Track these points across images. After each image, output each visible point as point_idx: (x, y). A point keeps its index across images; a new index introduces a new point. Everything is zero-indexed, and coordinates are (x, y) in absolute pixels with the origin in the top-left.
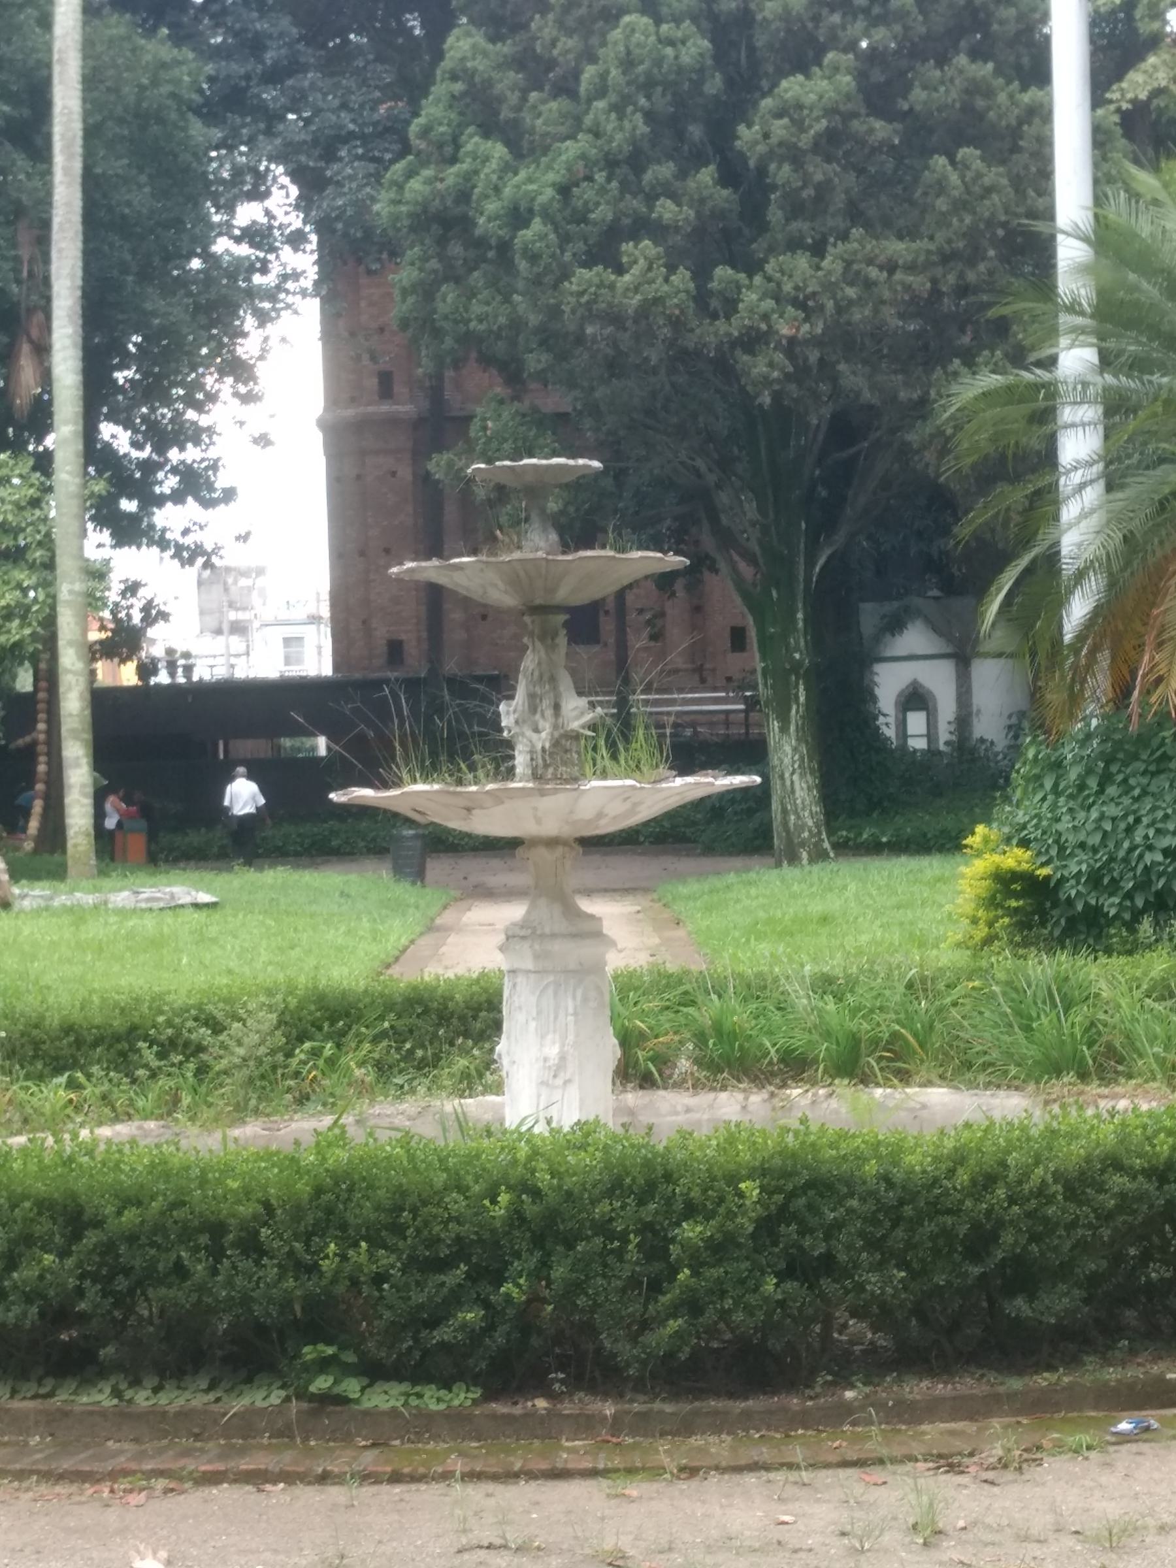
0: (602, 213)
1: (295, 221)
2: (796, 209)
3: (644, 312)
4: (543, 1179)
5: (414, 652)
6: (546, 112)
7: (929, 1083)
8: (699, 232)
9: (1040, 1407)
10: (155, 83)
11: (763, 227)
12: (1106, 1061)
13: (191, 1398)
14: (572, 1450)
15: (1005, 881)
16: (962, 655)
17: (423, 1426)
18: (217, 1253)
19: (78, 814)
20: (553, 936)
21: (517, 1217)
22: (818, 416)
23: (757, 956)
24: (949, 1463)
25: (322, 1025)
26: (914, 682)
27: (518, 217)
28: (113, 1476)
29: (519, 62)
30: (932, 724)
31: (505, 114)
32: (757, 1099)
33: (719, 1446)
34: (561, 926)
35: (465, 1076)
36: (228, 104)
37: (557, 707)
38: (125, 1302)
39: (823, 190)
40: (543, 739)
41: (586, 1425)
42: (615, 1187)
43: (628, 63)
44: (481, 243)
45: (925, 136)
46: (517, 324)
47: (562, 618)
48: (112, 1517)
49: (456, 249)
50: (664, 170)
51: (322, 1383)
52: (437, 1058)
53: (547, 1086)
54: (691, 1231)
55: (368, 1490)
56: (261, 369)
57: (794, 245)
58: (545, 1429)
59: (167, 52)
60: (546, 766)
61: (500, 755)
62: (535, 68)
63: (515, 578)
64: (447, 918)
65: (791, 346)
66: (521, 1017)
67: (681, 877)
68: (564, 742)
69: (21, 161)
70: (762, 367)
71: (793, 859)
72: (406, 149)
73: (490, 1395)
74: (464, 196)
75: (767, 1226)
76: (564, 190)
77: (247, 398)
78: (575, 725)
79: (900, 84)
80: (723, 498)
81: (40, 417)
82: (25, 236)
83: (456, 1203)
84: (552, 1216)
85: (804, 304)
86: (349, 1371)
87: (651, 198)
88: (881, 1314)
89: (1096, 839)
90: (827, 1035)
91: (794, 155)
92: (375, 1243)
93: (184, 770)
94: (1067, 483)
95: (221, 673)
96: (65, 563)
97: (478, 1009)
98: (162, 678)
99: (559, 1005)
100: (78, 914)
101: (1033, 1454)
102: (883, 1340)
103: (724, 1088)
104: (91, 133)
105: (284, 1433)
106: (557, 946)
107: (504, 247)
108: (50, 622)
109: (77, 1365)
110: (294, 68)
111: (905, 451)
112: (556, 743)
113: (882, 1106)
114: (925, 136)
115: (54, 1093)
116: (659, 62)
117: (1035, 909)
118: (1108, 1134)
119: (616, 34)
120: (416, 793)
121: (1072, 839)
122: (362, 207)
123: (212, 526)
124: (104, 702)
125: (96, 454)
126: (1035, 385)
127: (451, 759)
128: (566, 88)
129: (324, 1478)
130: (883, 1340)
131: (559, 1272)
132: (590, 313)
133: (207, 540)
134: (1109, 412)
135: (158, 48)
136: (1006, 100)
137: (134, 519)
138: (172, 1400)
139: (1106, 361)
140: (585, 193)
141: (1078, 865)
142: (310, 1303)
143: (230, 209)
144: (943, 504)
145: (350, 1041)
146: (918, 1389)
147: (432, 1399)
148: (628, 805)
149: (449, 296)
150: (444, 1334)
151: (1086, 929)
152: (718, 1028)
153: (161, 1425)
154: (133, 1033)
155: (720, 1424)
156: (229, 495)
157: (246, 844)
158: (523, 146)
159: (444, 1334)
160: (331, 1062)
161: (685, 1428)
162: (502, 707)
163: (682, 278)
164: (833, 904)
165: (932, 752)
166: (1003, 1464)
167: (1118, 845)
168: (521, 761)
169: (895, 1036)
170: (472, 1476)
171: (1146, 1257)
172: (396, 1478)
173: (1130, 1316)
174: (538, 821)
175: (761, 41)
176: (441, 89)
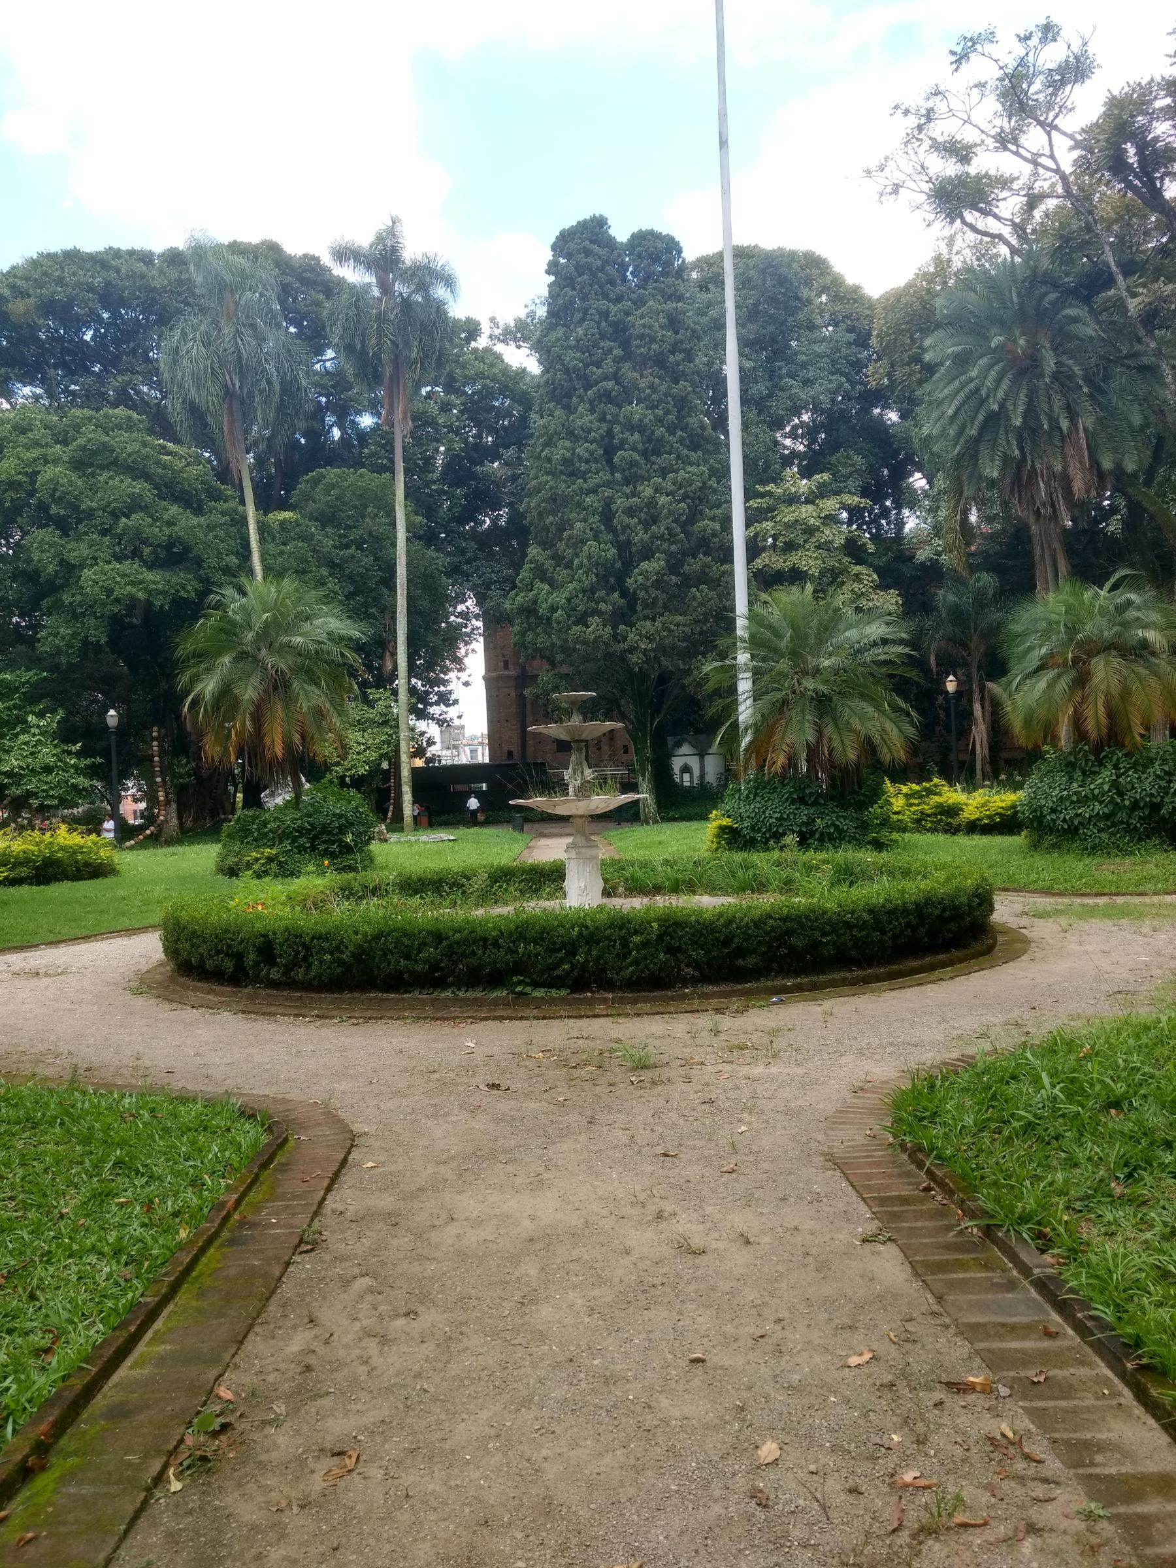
0: (582, 608)
4: (589, 923)
6: (562, 574)
8: (614, 614)
9: (747, 994)
11: (635, 612)
12: (760, 886)
14: (600, 1009)
15: (722, 829)
16: (702, 754)
17: (552, 1001)
21: (581, 935)
22: (654, 675)
23: (639, 855)
24: (718, 1011)
26: (687, 765)
28: (454, 1018)
29: (553, 557)
33: (646, 1007)
34: (584, 843)
36: (454, 571)
38: (455, 963)
39: (655, 599)
40: (578, 783)
41: (604, 1001)
42: (612, 925)
43: (590, 557)
44: (541, 618)
46: (553, 645)
48: (455, 1030)
49: (532, 620)
50: (602, 593)
51: (519, 988)
53: (581, 894)
54: (636, 939)
55: (535, 1022)
56: (466, 660)
57: (646, 618)
58: (591, 1003)
59: (434, 555)
61: (564, 788)
62: (558, 559)
63: (569, 731)
64: (532, 844)
65: (645, 652)
68: (585, 784)
69: (386, 591)
70: (635, 659)
72: (514, 586)
74: (535, 602)
75: (660, 937)
76: (569, 600)
79: (681, 563)
80: (623, 702)
81: (393, 676)
82: (387, 616)
83: (561, 930)
84: (592, 935)
85: (649, 638)
86: (527, 984)
87: (597, 603)
88: (697, 965)
91: (646, 588)
93: (444, 796)
94: (740, 699)
95: (449, 762)
96: (402, 726)
101: (747, 1008)
102: (697, 974)
107: (549, 619)
108: (397, 746)
109: (440, 983)
110: (476, 559)
111: (683, 687)
114: (688, 582)
115: (416, 900)
117: (732, 838)
118: (767, 907)
120: (538, 801)
122: (499, 605)
124: (415, 771)
125: (412, 691)
126: (213, 441)
128: (569, 566)
129: (521, 1018)
130: (697, 974)
131: (594, 952)
133: (448, 717)
134: (754, 674)
135: (431, 553)
136: (716, 569)
138: (471, 994)
139: (753, 657)
140: (576, 601)
142: (515, 963)
144: (695, 704)
146: (708, 989)
147: (554, 993)
149: (530, 636)
150: (558, 972)
151: (749, 844)
153: (468, 1002)
154: (441, 881)
155: (646, 1000)
157: (471, 820)
158: (554, 585)
159: (558, 972)
161: (635, 1001)
163: (608, 629)
164: (662, 837)
165: (692, 787)
168: (571, 790)
170: (569, 1017)
171: (779, 947)
172: (544, 1018)
173: (774, 965)
175: (634, 550)
176: (526, 567)
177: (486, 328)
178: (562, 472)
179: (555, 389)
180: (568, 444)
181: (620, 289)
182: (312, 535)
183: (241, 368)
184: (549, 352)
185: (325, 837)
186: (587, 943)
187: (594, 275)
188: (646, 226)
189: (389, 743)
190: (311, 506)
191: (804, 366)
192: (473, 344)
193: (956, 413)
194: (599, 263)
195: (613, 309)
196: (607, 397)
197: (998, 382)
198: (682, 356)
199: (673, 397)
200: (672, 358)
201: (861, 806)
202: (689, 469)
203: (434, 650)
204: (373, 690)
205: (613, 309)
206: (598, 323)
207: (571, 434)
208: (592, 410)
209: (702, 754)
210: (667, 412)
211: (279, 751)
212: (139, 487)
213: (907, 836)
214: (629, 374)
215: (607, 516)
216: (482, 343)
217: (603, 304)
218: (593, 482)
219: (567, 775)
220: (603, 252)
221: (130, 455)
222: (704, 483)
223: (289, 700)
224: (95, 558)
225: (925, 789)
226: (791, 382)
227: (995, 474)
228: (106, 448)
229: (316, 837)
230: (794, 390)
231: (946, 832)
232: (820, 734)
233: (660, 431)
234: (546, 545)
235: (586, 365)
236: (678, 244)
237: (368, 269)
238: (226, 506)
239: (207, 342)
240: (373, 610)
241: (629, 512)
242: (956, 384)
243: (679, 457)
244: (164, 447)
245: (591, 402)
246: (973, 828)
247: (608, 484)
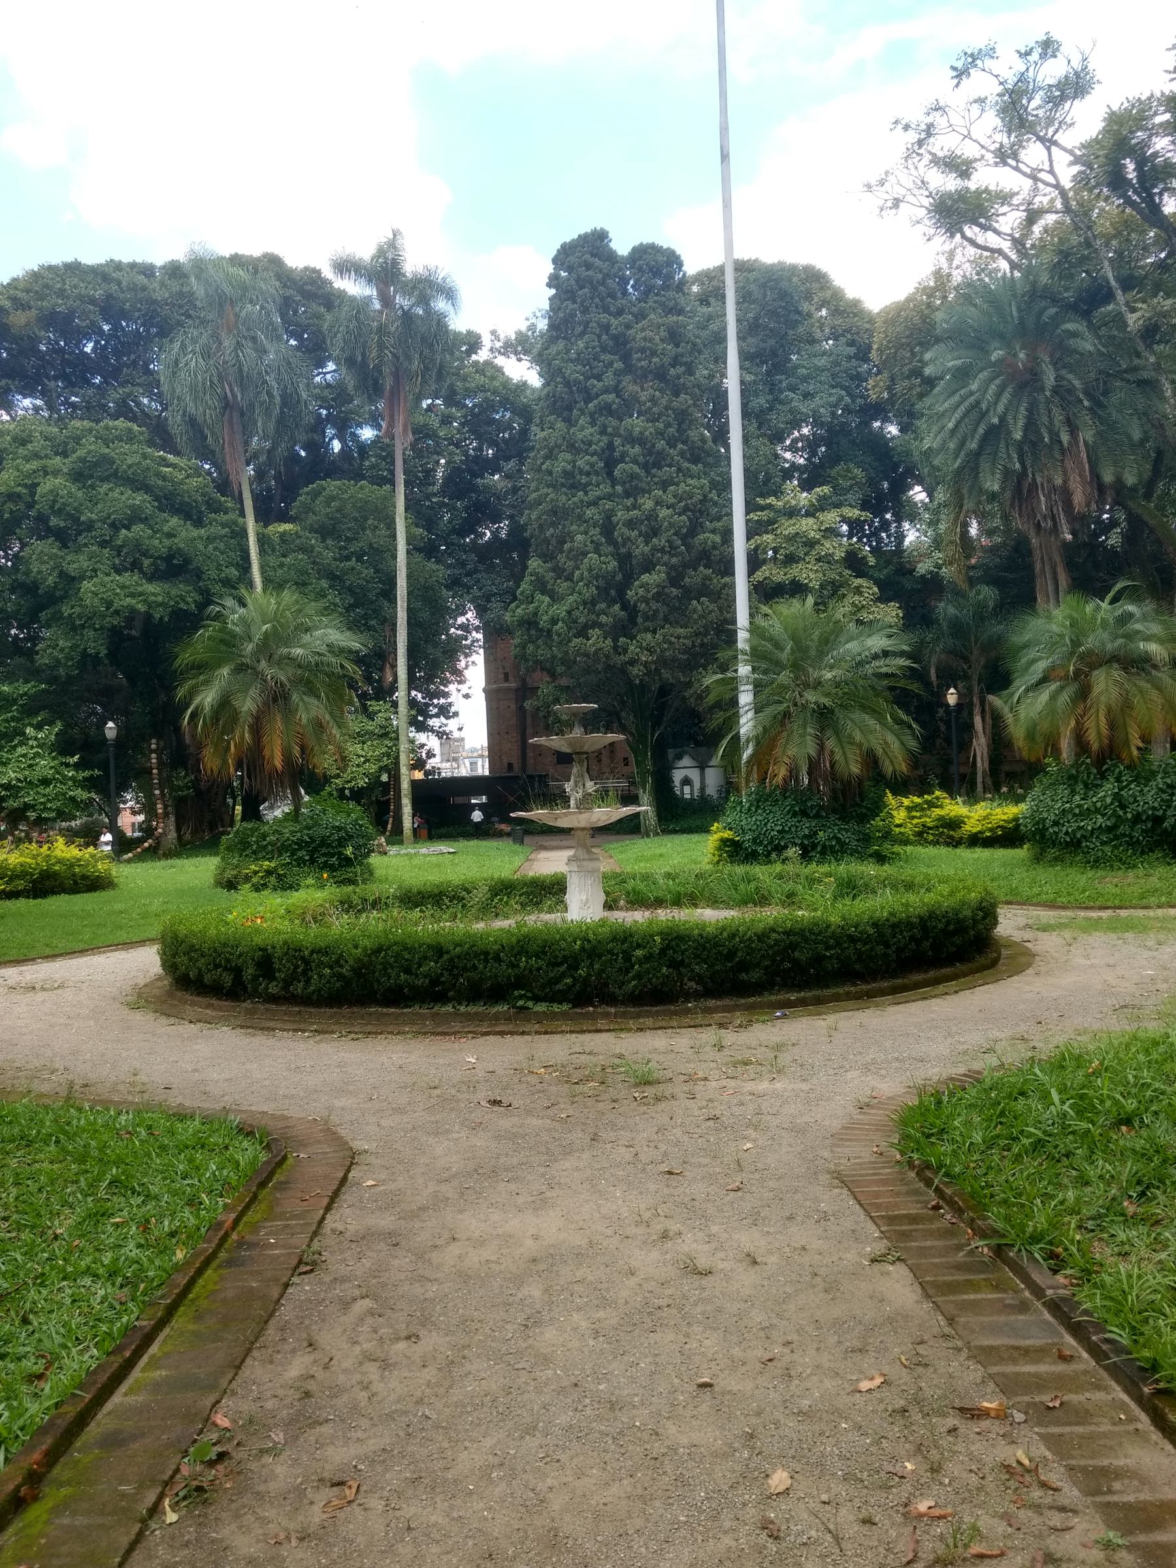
0: (582, 620)
1: (477, 622)
2: (647, 618)
3: (596, 652)
4: (591, 936)
5: (516, 767)
6: (563, 586)
8: (614, 626)
9: (750, 1008)
11: (635, 624)
12: (762, 900)
13: (478, 1008)
14: (602, 1023)
16: (702, 767)
17: (554, 1016)
18: (486, 961)
19: (407, 822)
21: (583, 949)
23: (640, 867)
24: (721, 1026)
25: (503, 890)
26: (687, 777)
27: (554, 621)
28: (455, 1033)
29: (553, 570)
32: (647, 913)
33: (649, 1022)
36: (454, 583)
38: (456, 977)
39: (656, 612)
40: (579, 796)
41: (606, 1015)
42: (614, 939)
43: (590, 570)
44: (542, 630)
45: (689, 594)
46: (554, 657)
48: (456, 1045)
49: (533, 632)
50: (603, 606)
51: (520, 1003)
53: (583, 907)
54: (639, 953)
56: (466, 672)
57: (647, 630)
58: (592, 1017)
61: (566, 800)
62: (559, 572)
67: (610, 842)
68: (587, 796)
69: (386, 603)
70: (635, 671)
71: (648, 836)
72: (515, 598)
73: (574, 1006)
74: (536, 614)
75: (663, 951)
76: (569, 612)
80: (623, 714)
81: (393, 688)
83: (563, 944)
84: (594, 948)
85: (650, 650)
86: (529, 999)
87: (598, 615)
88: (699, 979)
91: (646, 600)
92: (538, 957)
93: (444, 809)
94: (742, 711)
95: (449, 775)
96: (402, 738)
99: (585, 880)
102: (699, 988)
105: (509, 1019)
107: (549, 631)
108: (397, 758)
110: (476, 571)
111: (684, 699)
114: (689, 594)
115: (416, 913)
117: (733, 850)
118: (771, 921)
120: (539, 814)
122: (499, 617)
123: (452, 725)
124: (414, 783)
125: (412, 703)
129: (523, 1033)
130: (699, 988)
131: (597, 966)
132: (578, 653)
133: (447, 729)
134: (755, 686)
135: (431, 565)
136: (717, 582)
137: (423, 723)
138: (472, 1009)
139: (754, 670)
140: (576, 613)
144: (695, 716)
146: (711, 1003)
147: (556, 1008)
149: (531, 647)
150: (560, 987)
151: (751, 857)
152: (634, 890)
153: (469, 1017)
154: (441, 894)
155: (648, 1015)
156: (456, 714)
158: (555, 598)
159: (560, 987)
161: (638, 1016)
163: (609, 641)
164: (663, 850)
165: (692, 799)
166: (740, 1026)
168: (572, 802)
171: (782, 961)
172: (546, 1033)
175: (634, 562)
176: (527, 579)
178: (562, 485)
179: (555, 402)
180: (569, 457)
181: (621, 302)
182: (313, 546)
185: (324, 850)
186: (589, 957)
189: (388, 755)
190: (312, 519)
191: (805, 379)
192: (474, 357)
193: (956, 426)
194: (600, 276)
195: (614, 322)
196: (607, 409)
197: (998, 395)
198: (682, 369)
200: (672, 371)
201: (863, 819)
202: (690, 481)
203: (434, 662)
206: (599, 336)
207: (572, 447)
208: (593, 423)
210: (668, 425)
211: (278, 763)
212: (139, 498)
214: (630, 387)
215: (608, 529)
216: (482, 356)
217: (604, 318)
218: (594, 493)
219: (568, 787)
220: (605, 266)
221: (130, 467)
222: (705, 496)
223: (289, 713)
224: (95, 570)
225: (927, 802)
226: (791, 395)
227: (996, 487)
228: (106, 460)
229: (315, 850)
231: (948, 844)
232: (821, 747)
233: (661, 444)
234: (546, 557)
235: (587, 378)
236: (678, 257)
239: (206, 354)
240: (373, 622)
241: (631, 524)
242: (956, 398)
243: (679, 470)
244: (164, 459)
245: (592, 415)
246: (975, 841)
247: (609, 497)
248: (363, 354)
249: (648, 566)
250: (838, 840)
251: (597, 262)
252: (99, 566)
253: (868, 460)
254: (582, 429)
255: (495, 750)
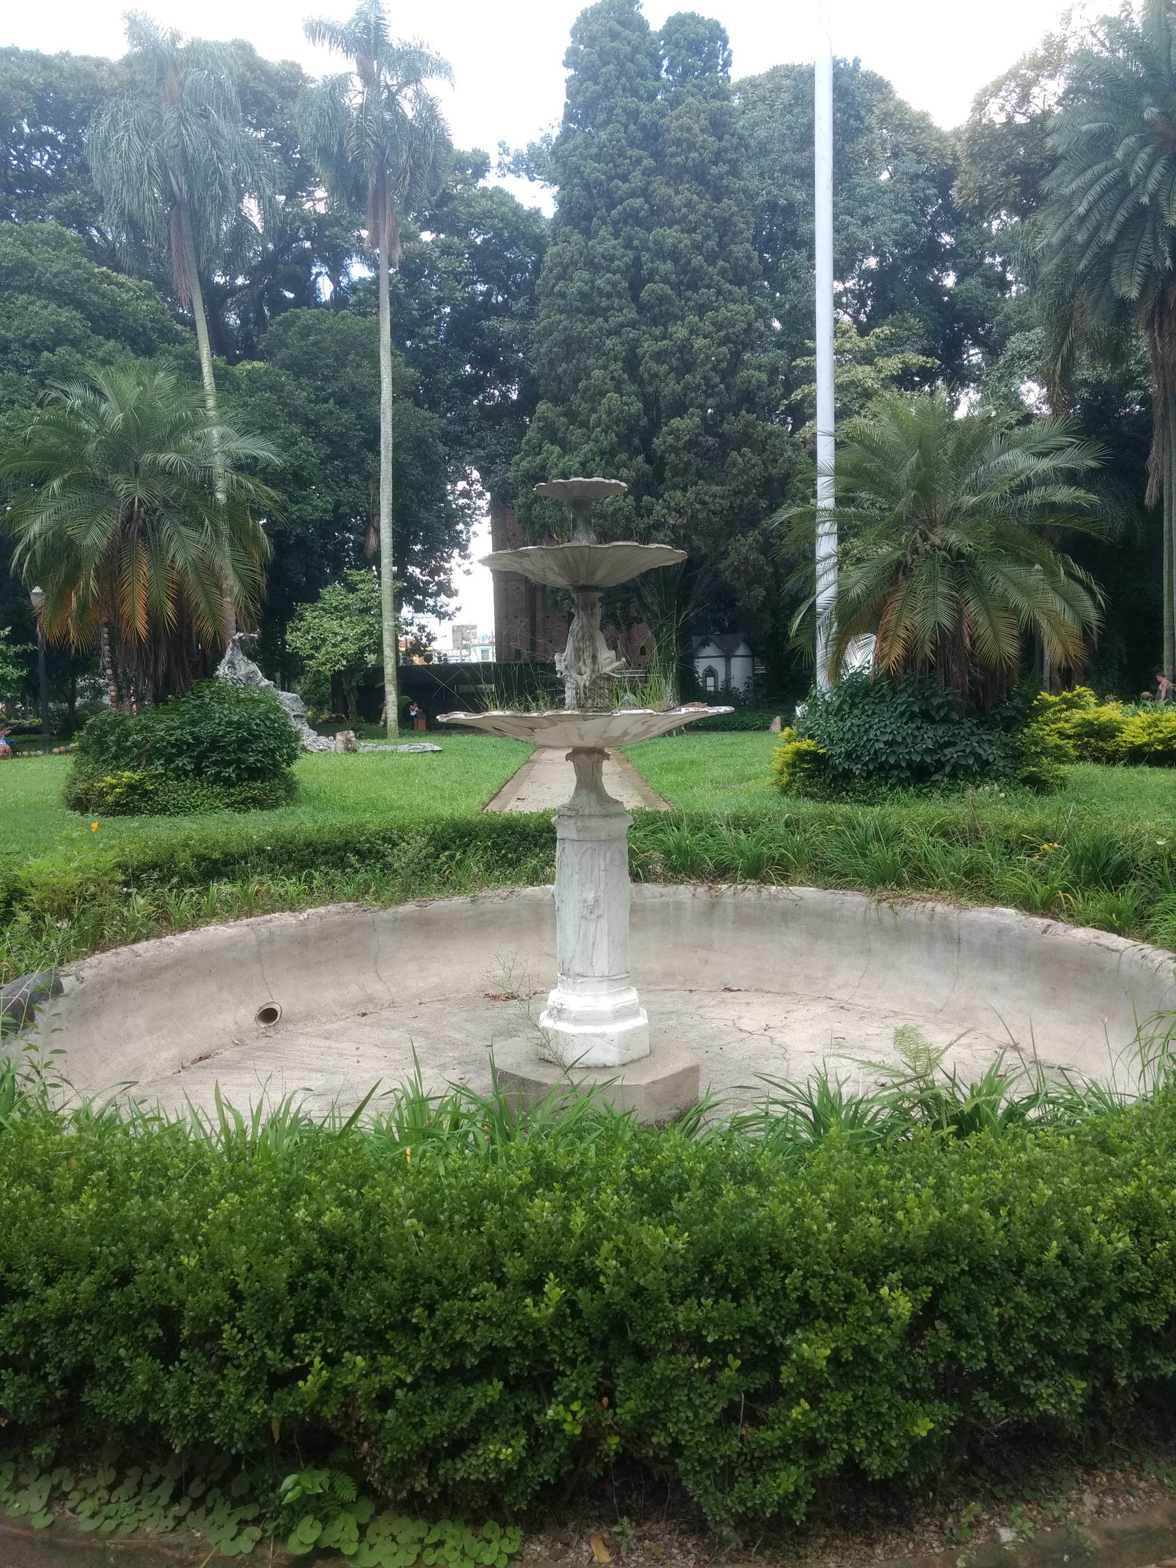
2: (676, 474)
6: (576, 434)
7: (801, 884)
10: (423, 426)
15: (800, 755)
16: (728, 657)
20: (591, 816)
29: (565, 415)
30: (716, 682)
31: (560, 435)
34: (596, 809)
35: (535, 871)
37: (594, 658)
39: (688, 464)
40: (585, 680)
43: (609, 412)
45: (728, 443)
47: (599, 595)
50: (624, 456)
52: (518, 860)
54: (813, 1349)
59: (428, 414)
60: (586, 698)
61: (554, 691)
62: (572, 416)
66: (568, 871)
69: (370, 455)
74: (543, 468)
77: (465, 557)
78: (607, 670)
89: (849, 736)
90: (742, 854)
91: (673, 449)
94: (820, 568)
97: (541, 832)
98: (435, 661)
100: (384, 754)
103: (682, 882)
104: (396, 447)
106: (594, 823)
112: (593, 683)
113: (776, 898)
114: (728, 443)
116: (622, 411)
117: (816, 773)
119: (604, 401)
121: (837, 736)
123: (450, 604)
127: (521, 694)
141: (840, 749)
143: (455, 483)
145: (471, 851)
148: (645, 727)
158: (567, 448)
160: (461, 861)
162: (557, 657)
163: (630, 499)
167: (861, 738)
168: (569, 695)
169: (782, 855)
174: (581, 737)
177: (494, 160)
178: (578, 310)
180: (586, 275)
181: (651, 84)
182: (283, 385)
183: (188, 166)
184: (565, 164)
185: (215, 757)
186: (599, 1346)
187: (620, 64)
188: (686, 9)
190: (283, 354)
191: (863, 202)
192: (482, 183)
193: (1089, 211)
194: (628, 49)
195: (644, 107)
196: (632, 217)
197: (1149, 167)
198: (726, 168)
199: (714, 219)
200: (714, 170)
201: (1011, 724)
202: (731, 306)
203: (427, 531)
204: (353, 572)
205: (644, 107)
206: (626, 127)
207: (592, 265)
208: (616, 235)
209: (728, 657)
210: (707, 237)
211: (141, 625)
212: (65, 315)
213: (1065, 769)
214: (662, 189)
215: (632, 362)
216: (490, 181)
217: (632, 102)
218: (615, 320)
219: (561, 662)
220: (634, 36)
221: (56, 275)
222: (750, 325)
223: (158, 551)
224: (12, 402)
225: (1065, 701)
226: (848, 218)
227: (1134, 294)
229: (202, 756)
230: (852, 229)
231: (1097, 760)
232: (959, 614)
233: (698, 260)
234: (558, 400)
236: (723, 31)
237: (347, 51)
238: (181, 349)
239: (144, 133)
240: (354, 477)
241: (659, 357)
242: (1089, 175)
243: (719, 292)
244: (108, 277)
246: (1137, 756)
247: (633, 325)
248: (341, 144)
249: (679, 408)
250: (978, 757)
251: (627, 33)
252: (15, 396)
253: (926, 310)
254: (604, 239)
255: (502, 639)
